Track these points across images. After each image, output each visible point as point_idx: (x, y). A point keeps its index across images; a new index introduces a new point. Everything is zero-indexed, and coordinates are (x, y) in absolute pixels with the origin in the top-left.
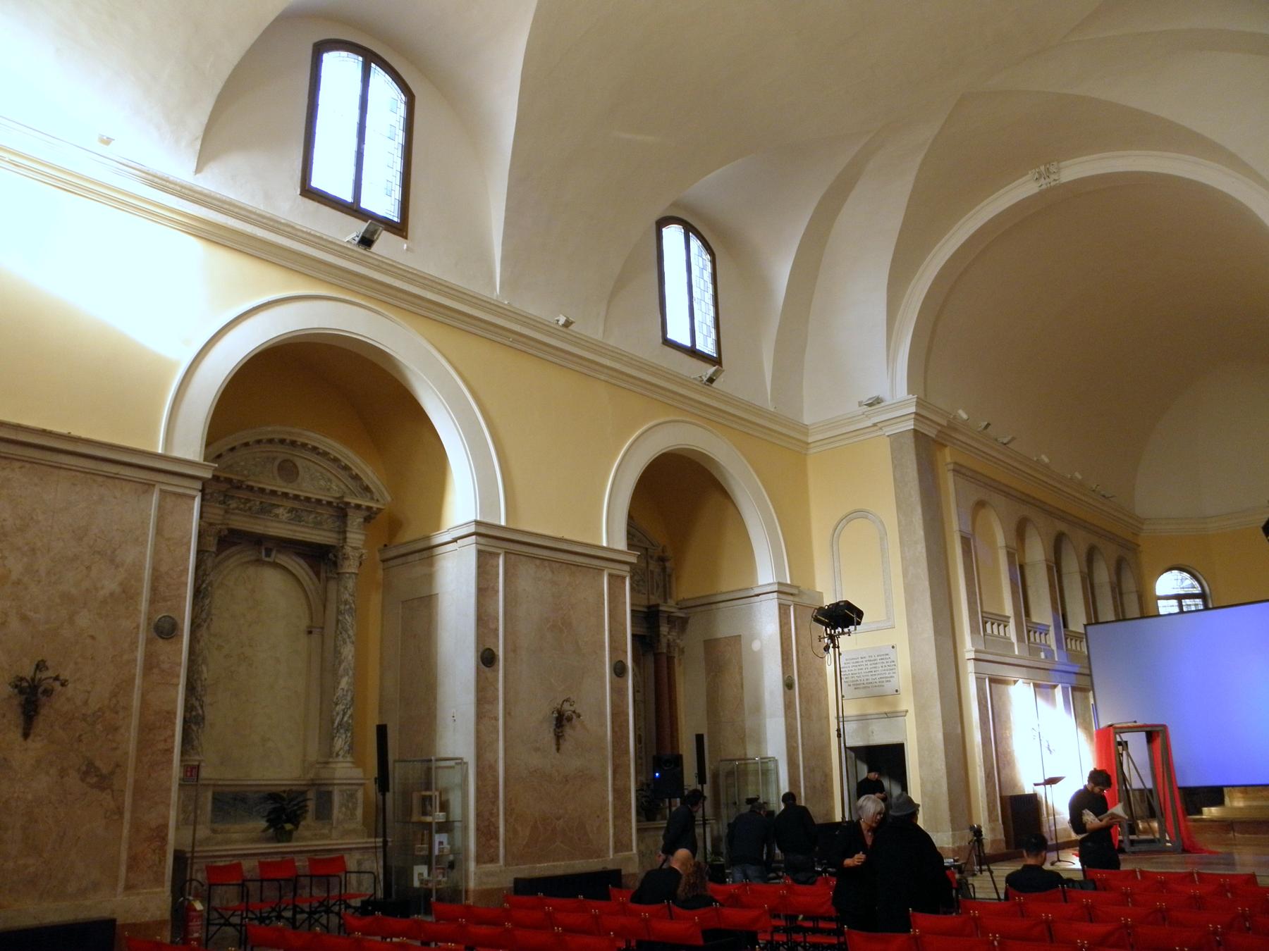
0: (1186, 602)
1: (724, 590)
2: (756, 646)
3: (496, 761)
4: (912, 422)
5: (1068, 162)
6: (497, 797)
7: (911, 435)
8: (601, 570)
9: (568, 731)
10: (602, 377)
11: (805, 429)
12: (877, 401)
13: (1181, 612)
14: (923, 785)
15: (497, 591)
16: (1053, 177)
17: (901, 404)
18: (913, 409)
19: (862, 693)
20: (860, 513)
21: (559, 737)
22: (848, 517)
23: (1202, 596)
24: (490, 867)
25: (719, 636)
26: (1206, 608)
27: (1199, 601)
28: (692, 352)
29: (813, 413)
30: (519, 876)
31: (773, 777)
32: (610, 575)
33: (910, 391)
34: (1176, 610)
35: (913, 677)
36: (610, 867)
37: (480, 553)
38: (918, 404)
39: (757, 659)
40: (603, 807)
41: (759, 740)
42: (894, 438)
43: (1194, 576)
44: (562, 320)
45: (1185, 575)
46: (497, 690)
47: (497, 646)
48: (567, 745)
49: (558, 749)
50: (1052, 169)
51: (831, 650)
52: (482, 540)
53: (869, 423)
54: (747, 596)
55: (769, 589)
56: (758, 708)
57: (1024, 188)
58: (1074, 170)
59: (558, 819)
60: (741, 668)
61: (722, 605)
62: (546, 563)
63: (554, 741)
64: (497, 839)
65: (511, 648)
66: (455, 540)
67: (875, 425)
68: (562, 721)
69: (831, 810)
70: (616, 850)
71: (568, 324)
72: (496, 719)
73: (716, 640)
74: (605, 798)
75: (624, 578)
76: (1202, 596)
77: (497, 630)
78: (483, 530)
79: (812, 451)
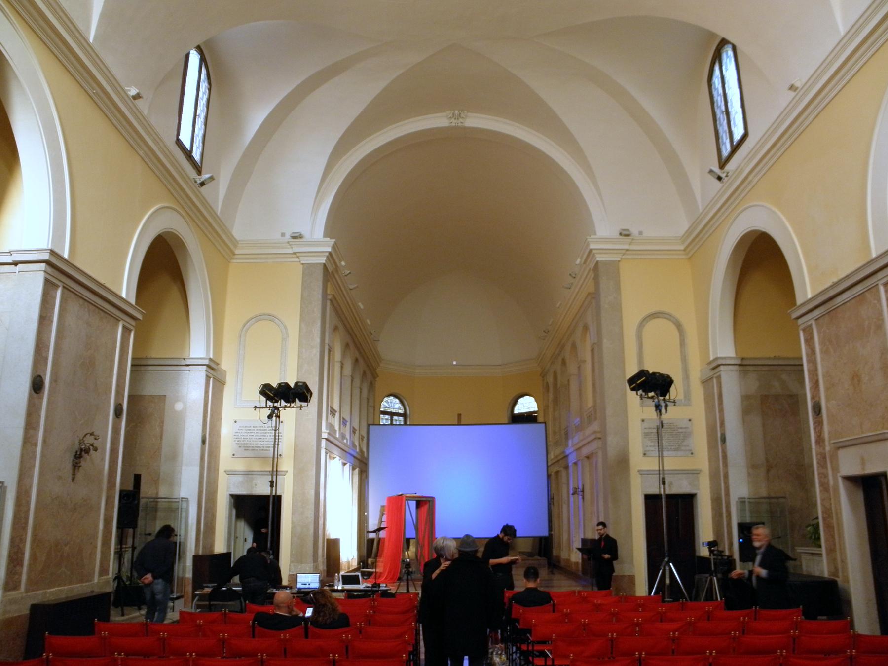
0: (395, 418)
1: (154, 355)
2: (179, 406)
3: (31, 487)
4: (325, 258)
5: (474, 115)
6: (26, 523)
7: (322, 267)
8: (118, 320)
9: (85, 463)
10: (141, 153)
11: (236, 243)
12: (297, 237)
13: (391, 424)
14: (293, 528)
15: (52, 322)
16: (461, 120)
17: (317, 243)
18: (329, 249)
19: (247, 454)
20: (269, 317)
21: (76, 466)
22: (258, 318)
23: (404, 415)
24: (13, 594)
25: (144, 393)
26: (405, 424)
27: (401, 418)
28: (188, 154)
29: (240, 230)
30: (35, 602)
31: (184, 514)
32: (124, 327)
33: (328, 233)
34: (389, 422)
35: (296, 446)
36: (97, 590)
37: (47, 281)
38: (333, 247)
39: (180, 418)
40: (95, 536)
41: (172, 481)
42: (308, 269)
43: (402, 402)
44: (133, 92)
45: (397, 401)
46: (40, 416)
47: (45, 375)
48: (80, 475)
49: (73, 479)
50: (462, 115)
51: (274, 418)
52: (50, 270)
53: (290, 251)
54: (180, 364)
55: (200, 362)
56: (174, 456)
57: (439, 121)
58: (475, 121)
59: (66, 545)
60: (162, 422)
61: (150, 368)
62: (86, 304)
63: (71, 471)
64: (22, 565)
65: (55, 379)
66: (16, 264)
67: (295, 253)
68: (80, 454)
69: (823, 572)
70: (101, 574)
71: (137, 97)
72: (36, 445)
73: (141, 396)
74: (97, 526)
75: (130, 331)
76: (404, 415)
77: (47, 358)
78: (54, 261)
79: (235, 261)
